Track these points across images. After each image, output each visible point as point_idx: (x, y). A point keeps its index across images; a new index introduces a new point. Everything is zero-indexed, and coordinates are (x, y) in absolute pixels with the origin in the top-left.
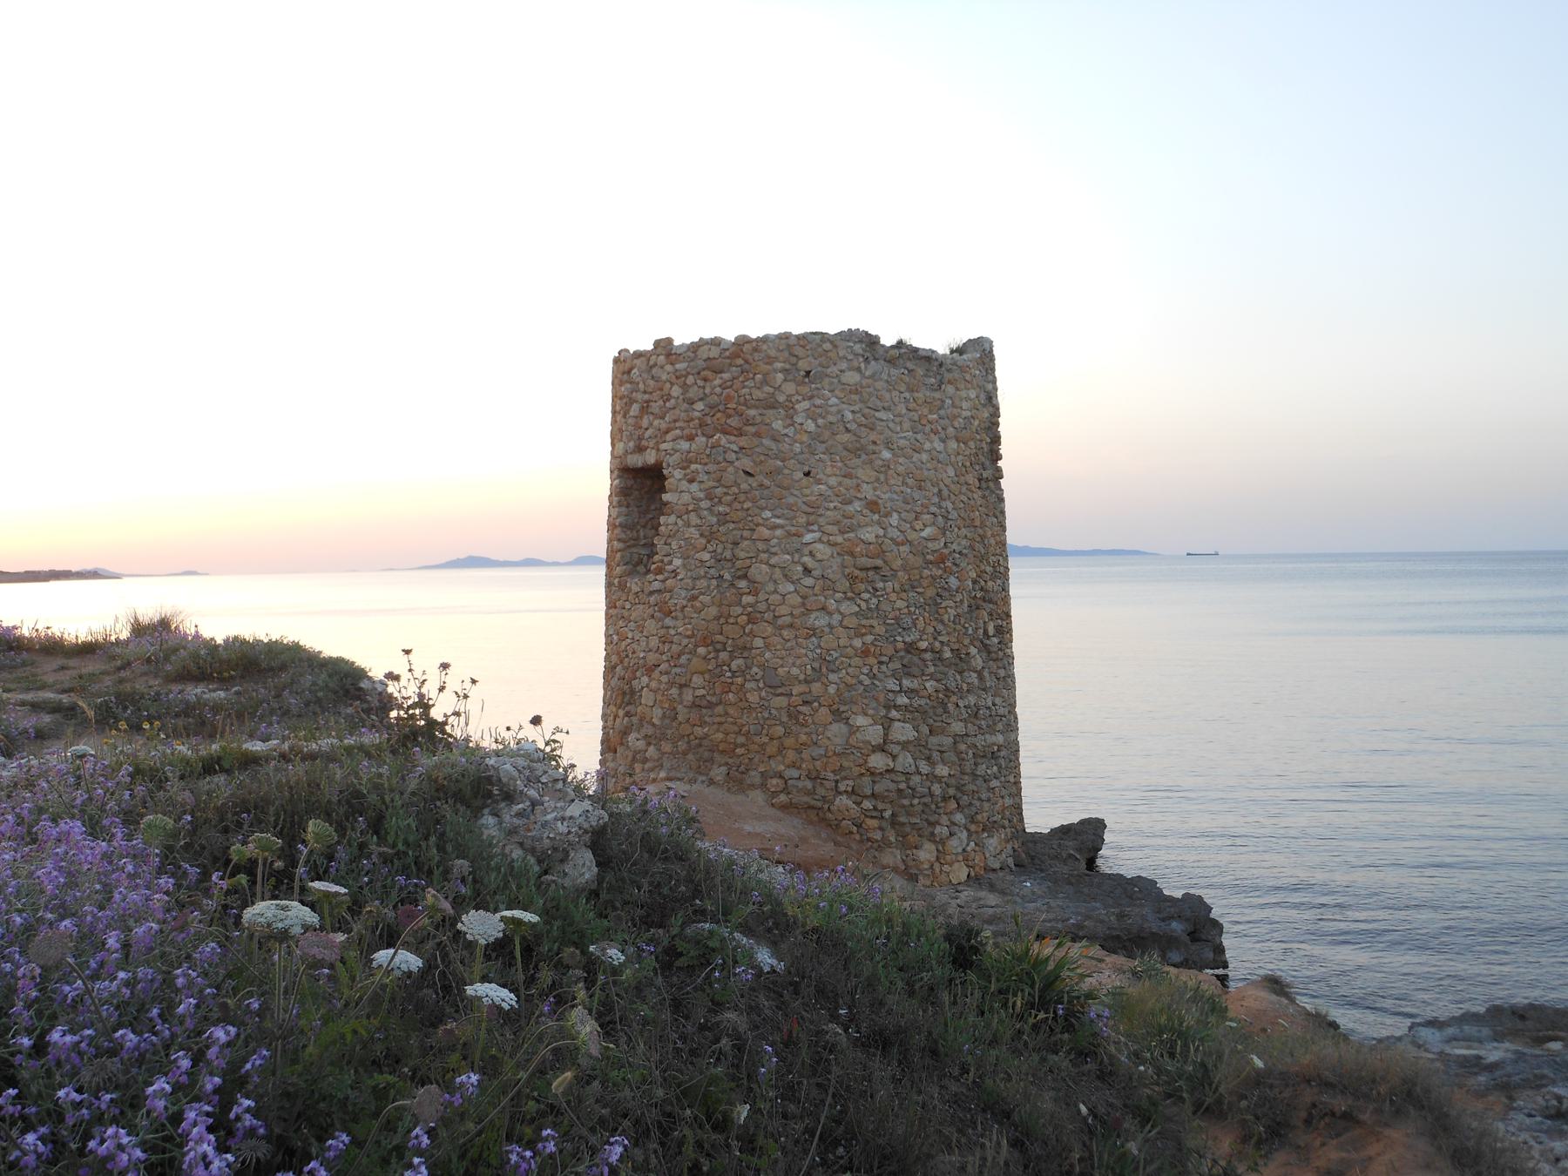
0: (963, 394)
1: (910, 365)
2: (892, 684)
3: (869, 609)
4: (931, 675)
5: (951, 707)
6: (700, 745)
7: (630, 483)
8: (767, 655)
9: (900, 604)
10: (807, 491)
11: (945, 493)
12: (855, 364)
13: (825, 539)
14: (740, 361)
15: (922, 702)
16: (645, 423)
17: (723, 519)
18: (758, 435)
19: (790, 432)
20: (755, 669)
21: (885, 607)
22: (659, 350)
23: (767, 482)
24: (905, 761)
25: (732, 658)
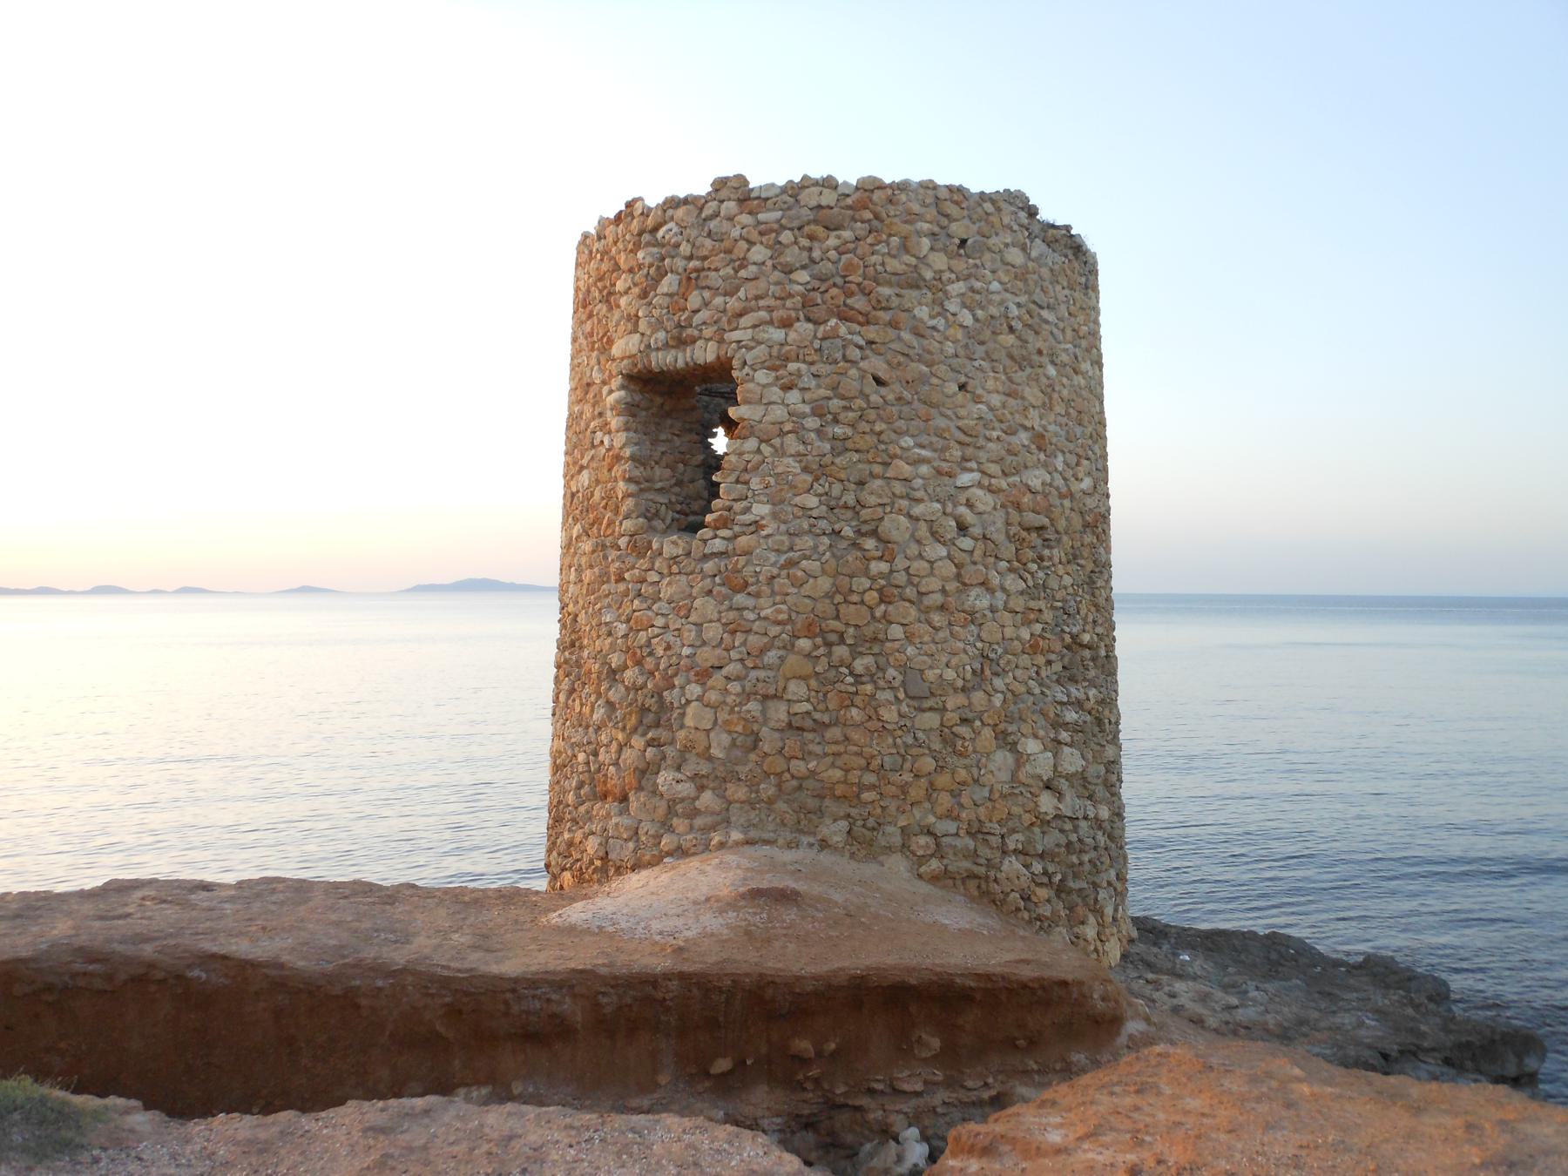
6: (800, 788)
7: (638, 397)
8: (910, 650)
10: (962, 412)
14: (868, 215)
16: (694, 300)
17: (841, 446)
18: (894, 325)
19: (940, 323)
20: (891, 672)
21: (1053, 583)
22: (723, 194)
23: (907, 395)
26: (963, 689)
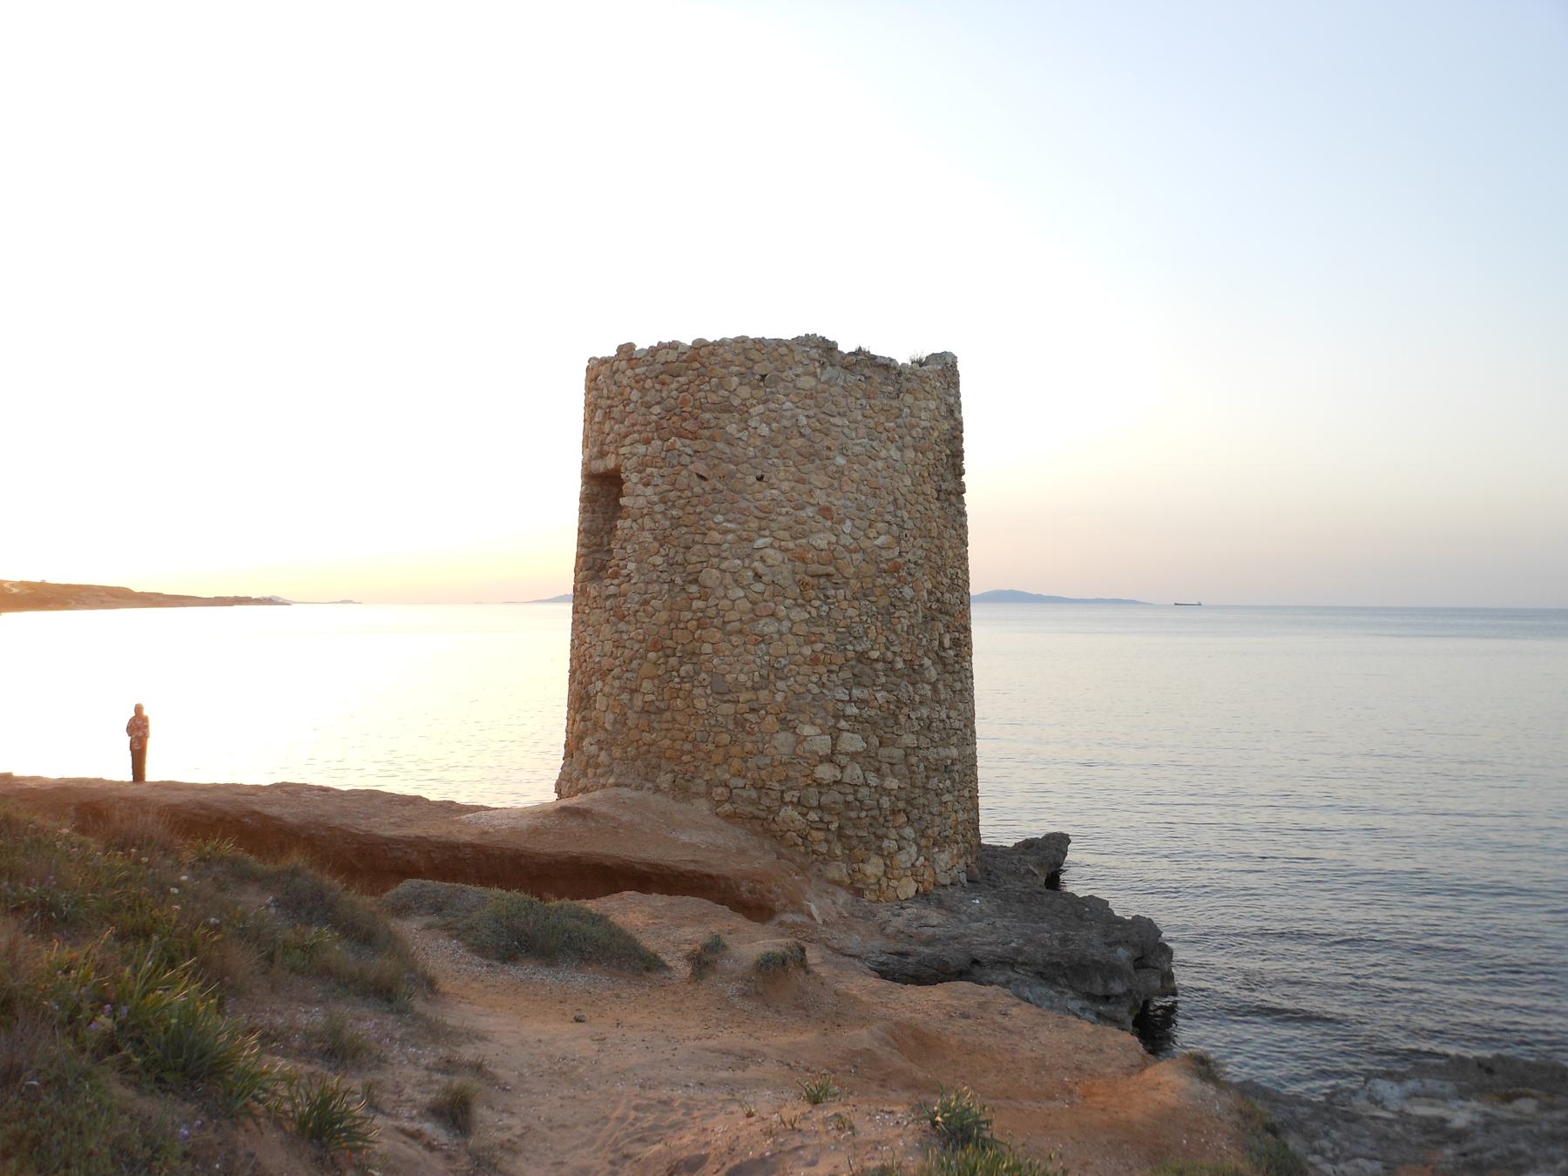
0: (923, 404)
1: (867, 372)
2: (841, 694)
3: (820, 616)
4: (882, 685)
5: (902, 719)
9: (851, 612)
10: (760, 496)
11: (901, 501)
12: (811, 368)
13: (776, 544)
15: (873, 713)
17: (676, 523)
18: (712, 439)
20: (703, 675)
21: (836, 614)
23: (719, 486)
24: (854, 772)
25: (681, 664)
26: (753, 688)
